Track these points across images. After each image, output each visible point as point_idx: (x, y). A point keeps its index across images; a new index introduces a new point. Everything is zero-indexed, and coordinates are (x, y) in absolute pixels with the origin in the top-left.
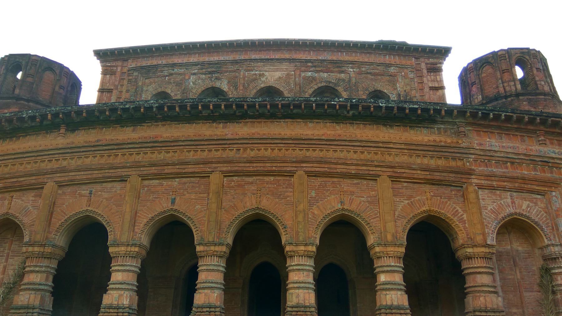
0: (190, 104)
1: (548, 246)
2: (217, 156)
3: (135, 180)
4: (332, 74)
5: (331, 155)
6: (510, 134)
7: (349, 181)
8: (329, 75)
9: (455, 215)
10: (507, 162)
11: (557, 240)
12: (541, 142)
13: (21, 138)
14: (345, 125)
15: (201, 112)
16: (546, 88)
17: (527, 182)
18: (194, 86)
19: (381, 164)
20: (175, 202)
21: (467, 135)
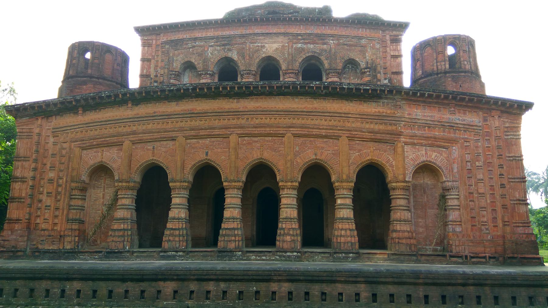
0: (214, 86)
1: (445, 181)
2: (234, 123)
3: (181, 140)
4: (317, 45)
5: (309, 122)
6: (431, 106)
7: (321, 140)
8: (315, 46)
9: (387, 162)
10: (425, 127)
11: (451, 178)
12: (451, 112)
13: (102, 110)
14: (320, 100)
15: (221, 92)
16: (468, 67)
17: (437, 140)
18: (212, 56)
19: (342, 129)
20: (208, 154)
21: (401, 107)
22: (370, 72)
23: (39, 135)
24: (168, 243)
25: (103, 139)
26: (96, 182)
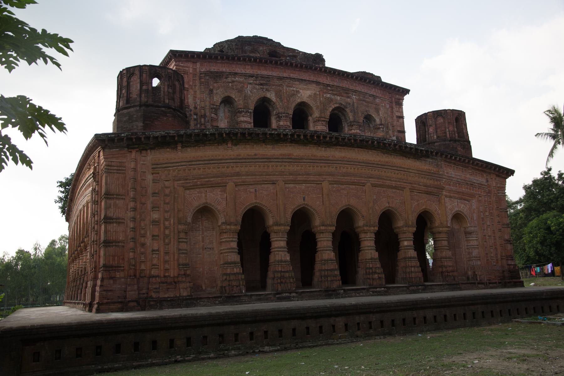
4: (342, 98)
7: (391, 190)
8: (341, 98)
18: (251, 94)
22: (383, 128)
24: (280, 285)
25: (207, 180)
26: (194, 225)
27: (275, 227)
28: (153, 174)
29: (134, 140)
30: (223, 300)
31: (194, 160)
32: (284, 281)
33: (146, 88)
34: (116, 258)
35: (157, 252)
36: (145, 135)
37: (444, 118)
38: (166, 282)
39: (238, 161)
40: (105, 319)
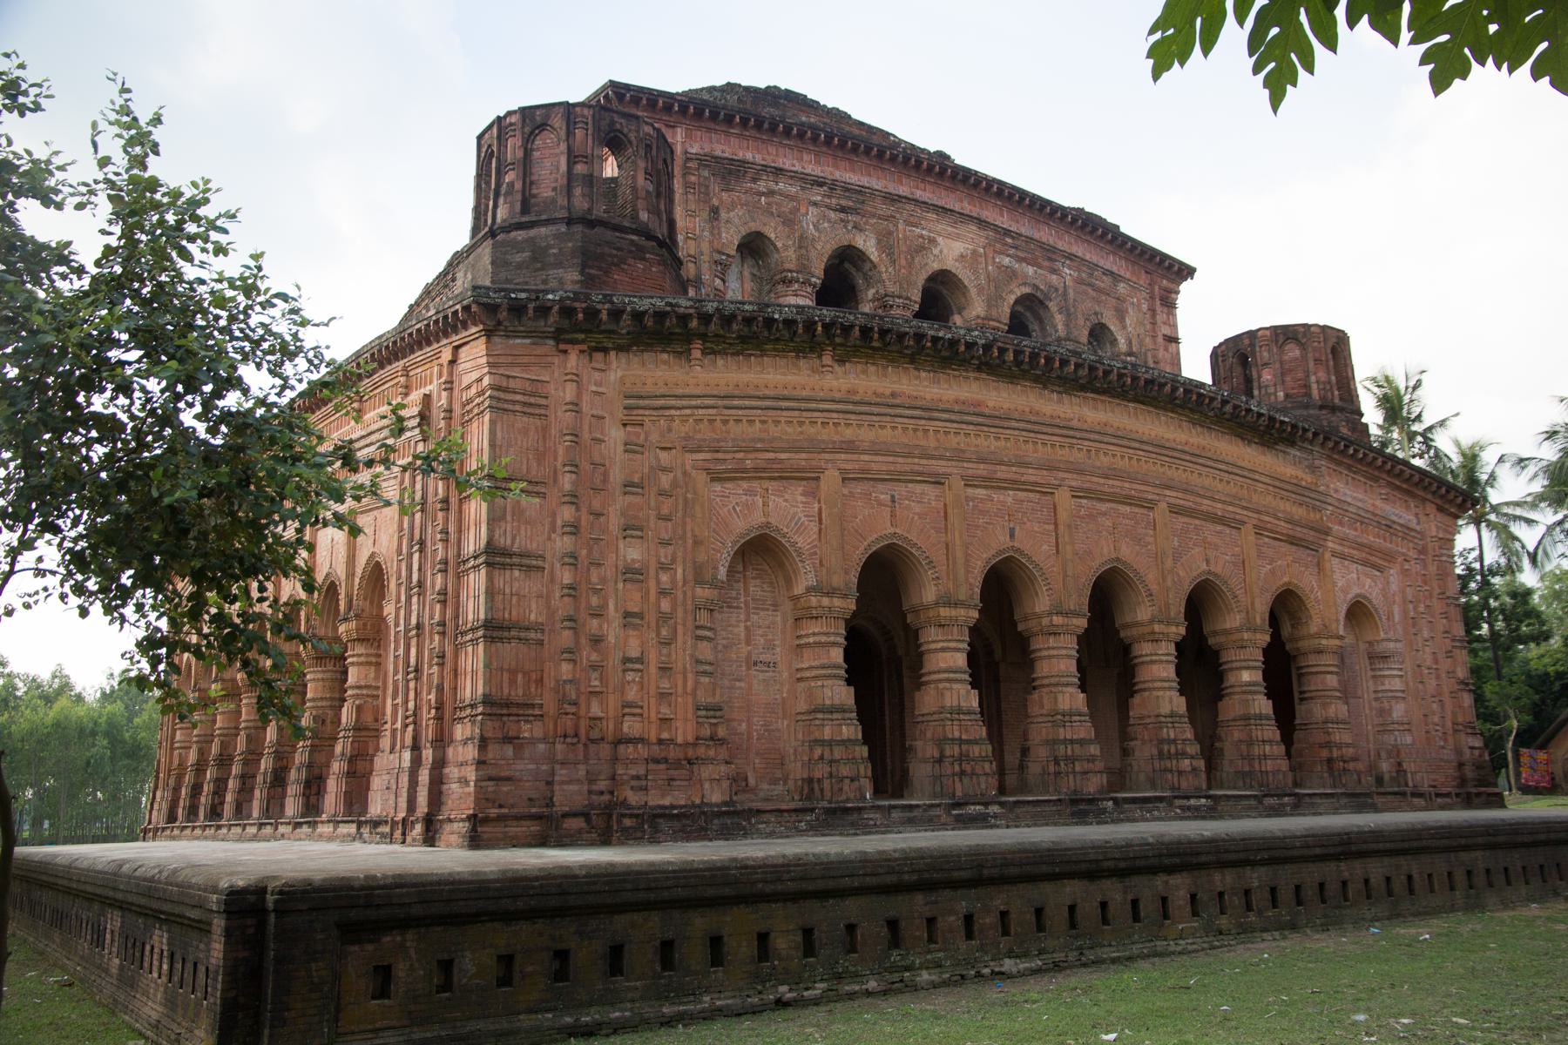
4: (1039, 271)
7: (1210, 525)
23: (575, 407)
25: (771, 455)
27: (942, 609)
28: (625, 425)
29: (581, 316)
30: (817, 819)
31: (736, 393)
32: (968, 769)
33: (585, 172)
34: (520, 676)
35: (638, 666)
36: (612, 303)
37: (1302, 346)
38: (666, 760)
39: (850, 407)
40: (582, 867)
